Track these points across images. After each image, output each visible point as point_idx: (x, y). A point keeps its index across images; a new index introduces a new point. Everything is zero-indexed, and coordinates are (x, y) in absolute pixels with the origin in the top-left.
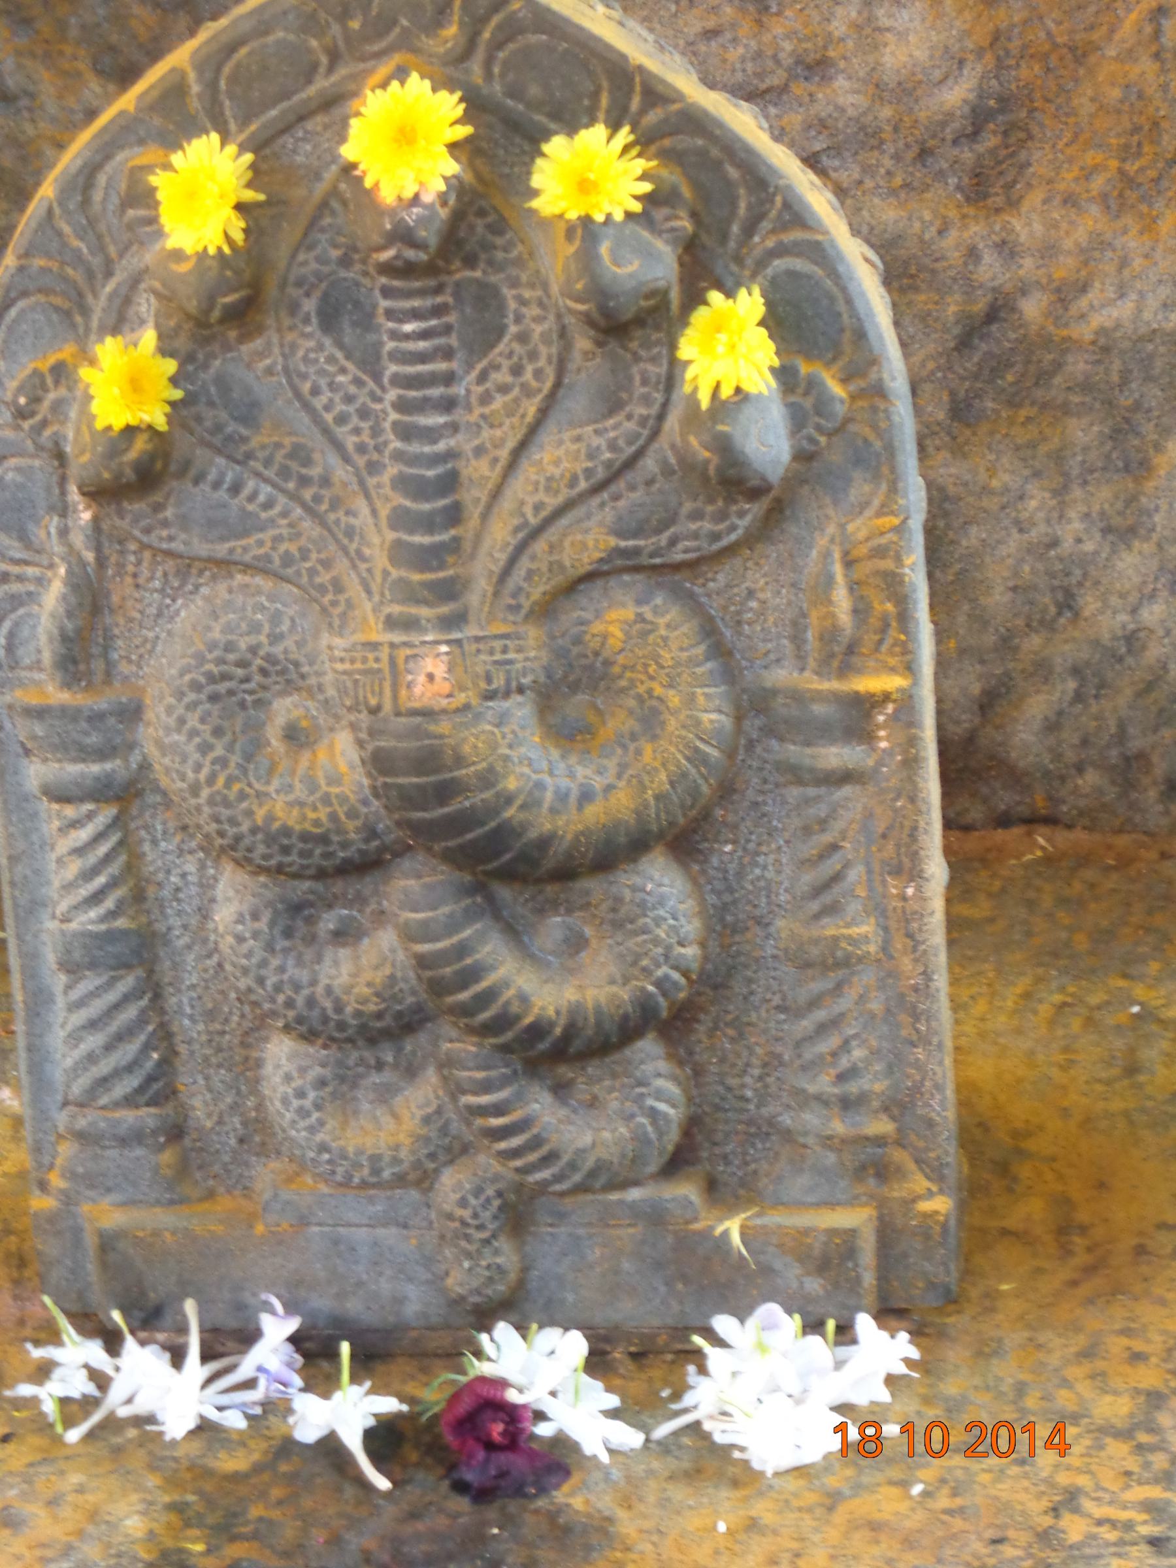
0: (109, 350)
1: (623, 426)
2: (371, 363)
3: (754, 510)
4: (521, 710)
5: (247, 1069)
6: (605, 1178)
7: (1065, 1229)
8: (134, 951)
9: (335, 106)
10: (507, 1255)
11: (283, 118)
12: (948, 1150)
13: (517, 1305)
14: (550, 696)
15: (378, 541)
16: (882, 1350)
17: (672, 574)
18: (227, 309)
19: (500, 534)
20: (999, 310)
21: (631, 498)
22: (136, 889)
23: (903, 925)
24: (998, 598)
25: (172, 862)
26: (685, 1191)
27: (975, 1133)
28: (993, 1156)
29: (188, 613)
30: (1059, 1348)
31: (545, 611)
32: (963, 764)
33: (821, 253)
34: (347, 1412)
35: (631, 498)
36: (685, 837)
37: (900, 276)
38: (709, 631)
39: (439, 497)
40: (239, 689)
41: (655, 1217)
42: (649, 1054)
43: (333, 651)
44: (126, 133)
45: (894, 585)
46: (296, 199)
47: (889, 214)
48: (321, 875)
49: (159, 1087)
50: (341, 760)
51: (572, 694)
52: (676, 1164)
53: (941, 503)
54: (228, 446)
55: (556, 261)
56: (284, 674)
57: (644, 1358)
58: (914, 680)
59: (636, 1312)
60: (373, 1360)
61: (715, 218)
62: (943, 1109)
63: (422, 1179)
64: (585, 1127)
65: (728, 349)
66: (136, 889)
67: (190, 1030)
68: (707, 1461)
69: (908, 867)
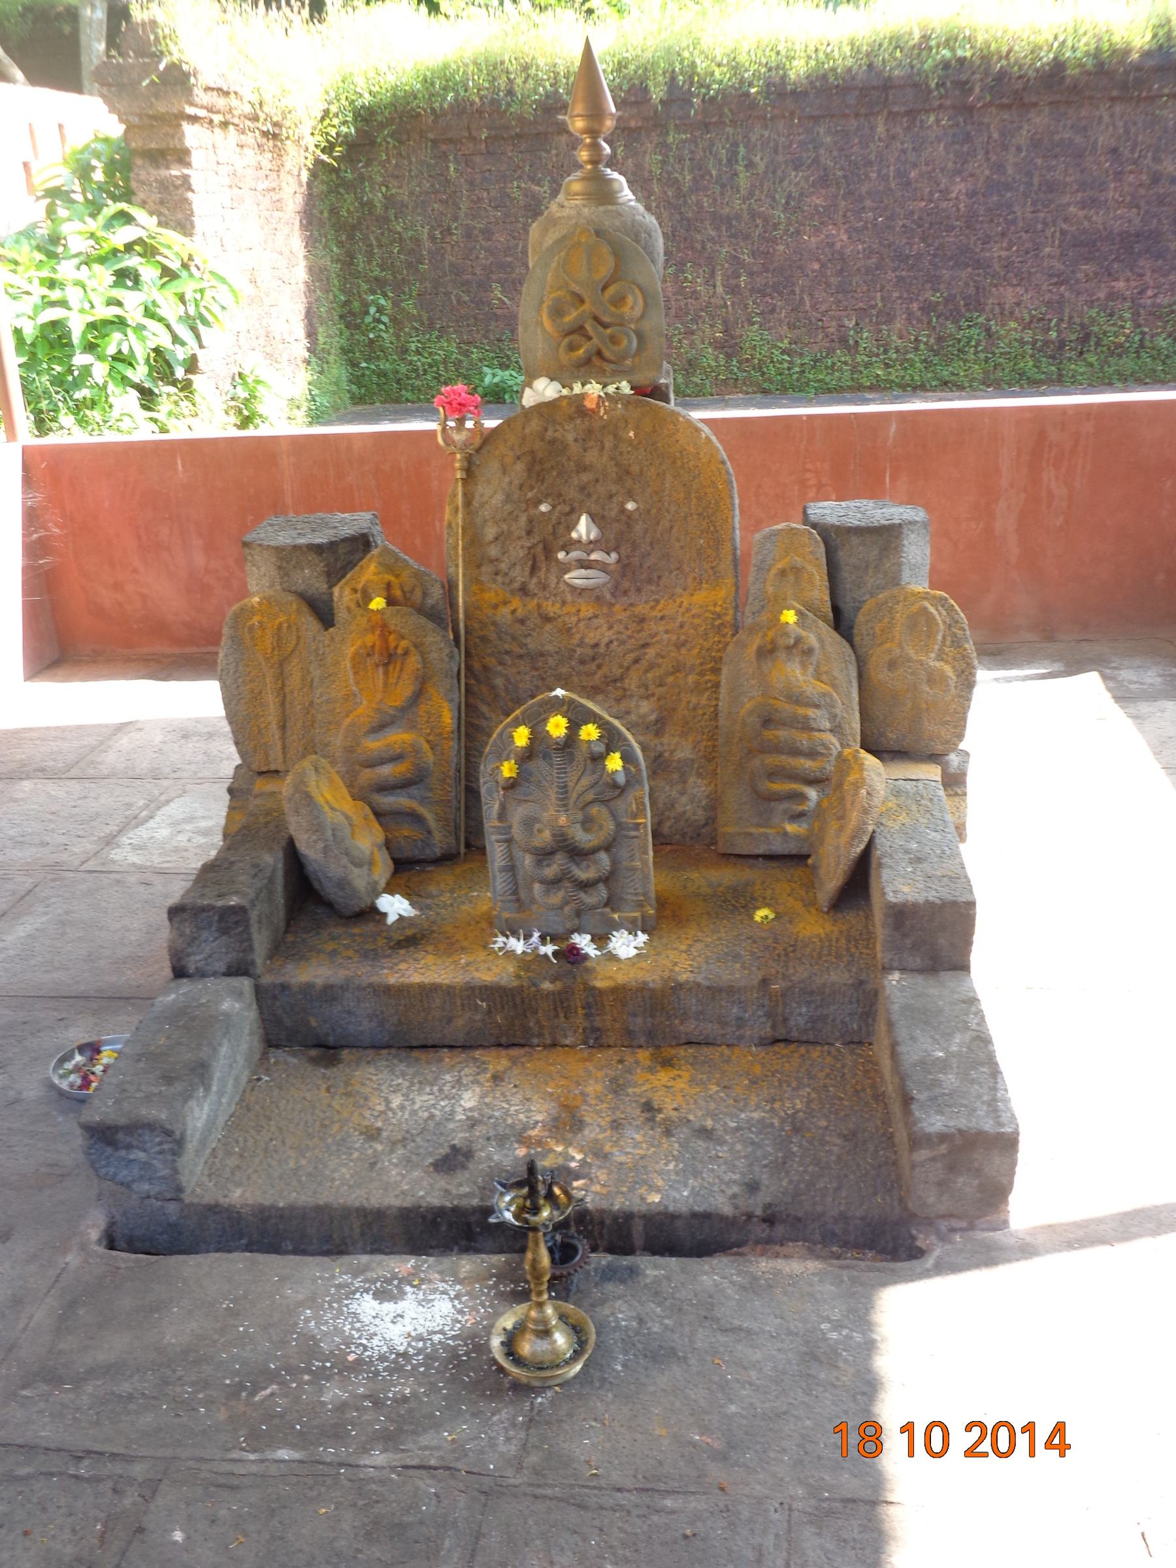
0: (506, 764)
1: (596, 776)
2: (551, 765)
3: (617, 792)
4: (578, 826)
5: (531, 889)
6: (594, 908)
7: (674, 916)
8: (511, 868)
9: (545, 721)
10: (576, 922)
11: (536, 723)
12: (654, 902)
13: (579, 930)
14: (583, 823)
15: (553, 796)
16: (642, 938)
17: (604, 802)
18: (527, 756)
19: (575, 795)
20: (661, 755)
21: (598, 789)
22: (511, 857)
23: (645, 863)
24: (661, 805)
25: (517, 853)
26: (608, 910)
27: (658, 899)
28: (662, 903)
29: (520, 809)
30: (674, 937)
31: (583, 809)
32: (655, 834)
33: (630, 745)
34: (549, 949)
35: (598, 789)
36: (607, 848)
37: (644, 749)
38: (611, 812)
39: (564, 790)
40: (529, 823)
41: (602, 914)
42: (601, 886)
43: (546, 816)
44: (508, 726)
45: (643, 804)
46: (538, 736)
47: (641, 738)
48: (544, 855)
49: (515, 892)
50: (547, 835)
51: (587, 823)
52: (606, 905)
53: (651, 789)
54: (527, 780)
55: (584, 747)
56: (537, 820)
57: (600, 939)
58: (647, 820)
59: (599, 931)
60: (553, 941)
61: (611, 740)
62: (653, 895)
63: (561, 908)
64: (590, 899)
65: (614, 763)
66: (511, 857)
67: (521, 882)
68: (612, 957)
69: (646, 853)
